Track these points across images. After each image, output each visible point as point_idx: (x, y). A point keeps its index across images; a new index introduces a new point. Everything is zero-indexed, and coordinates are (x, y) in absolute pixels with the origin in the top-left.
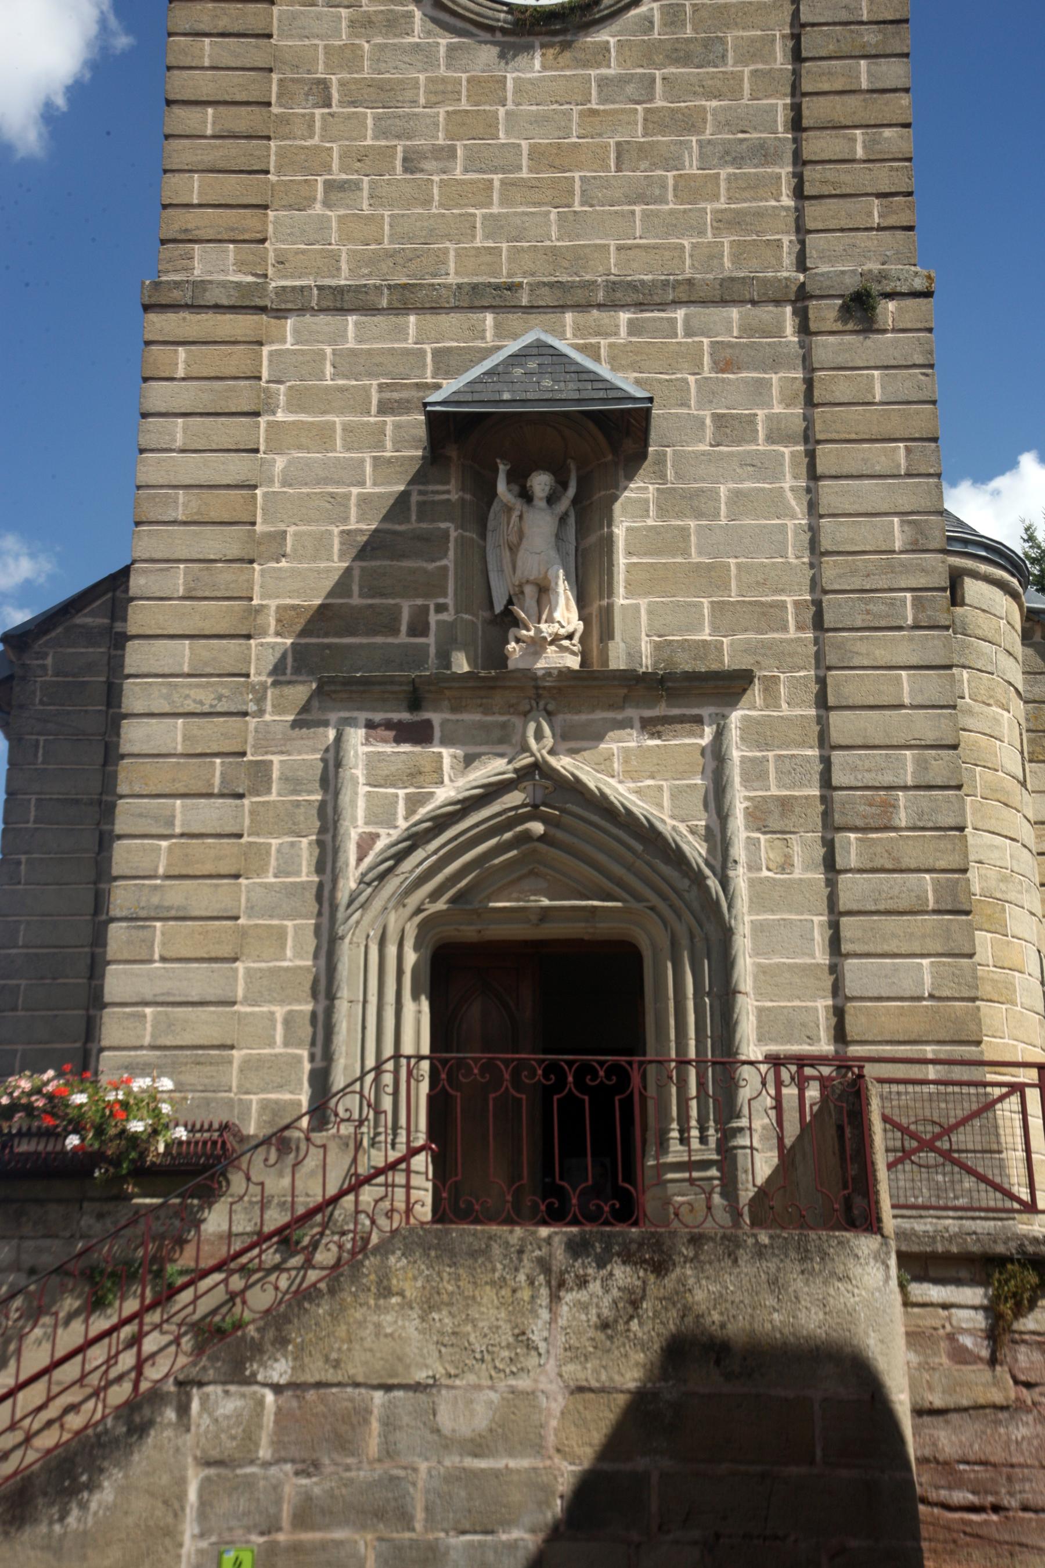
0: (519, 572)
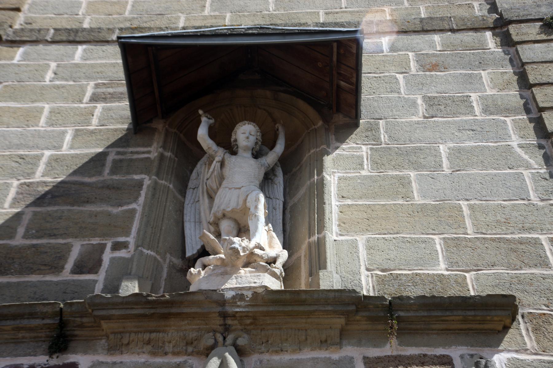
0: (215, 209)
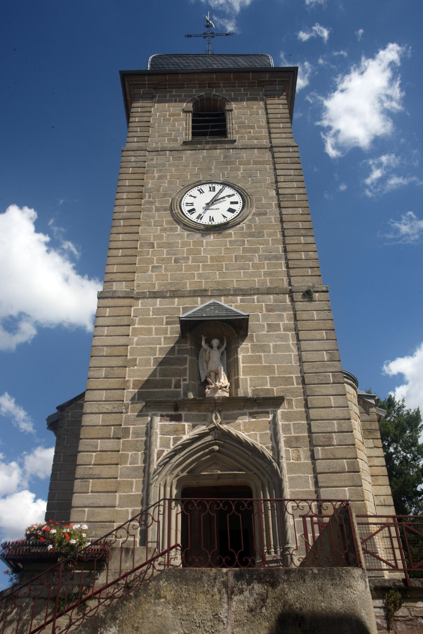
0: (209, 369)
